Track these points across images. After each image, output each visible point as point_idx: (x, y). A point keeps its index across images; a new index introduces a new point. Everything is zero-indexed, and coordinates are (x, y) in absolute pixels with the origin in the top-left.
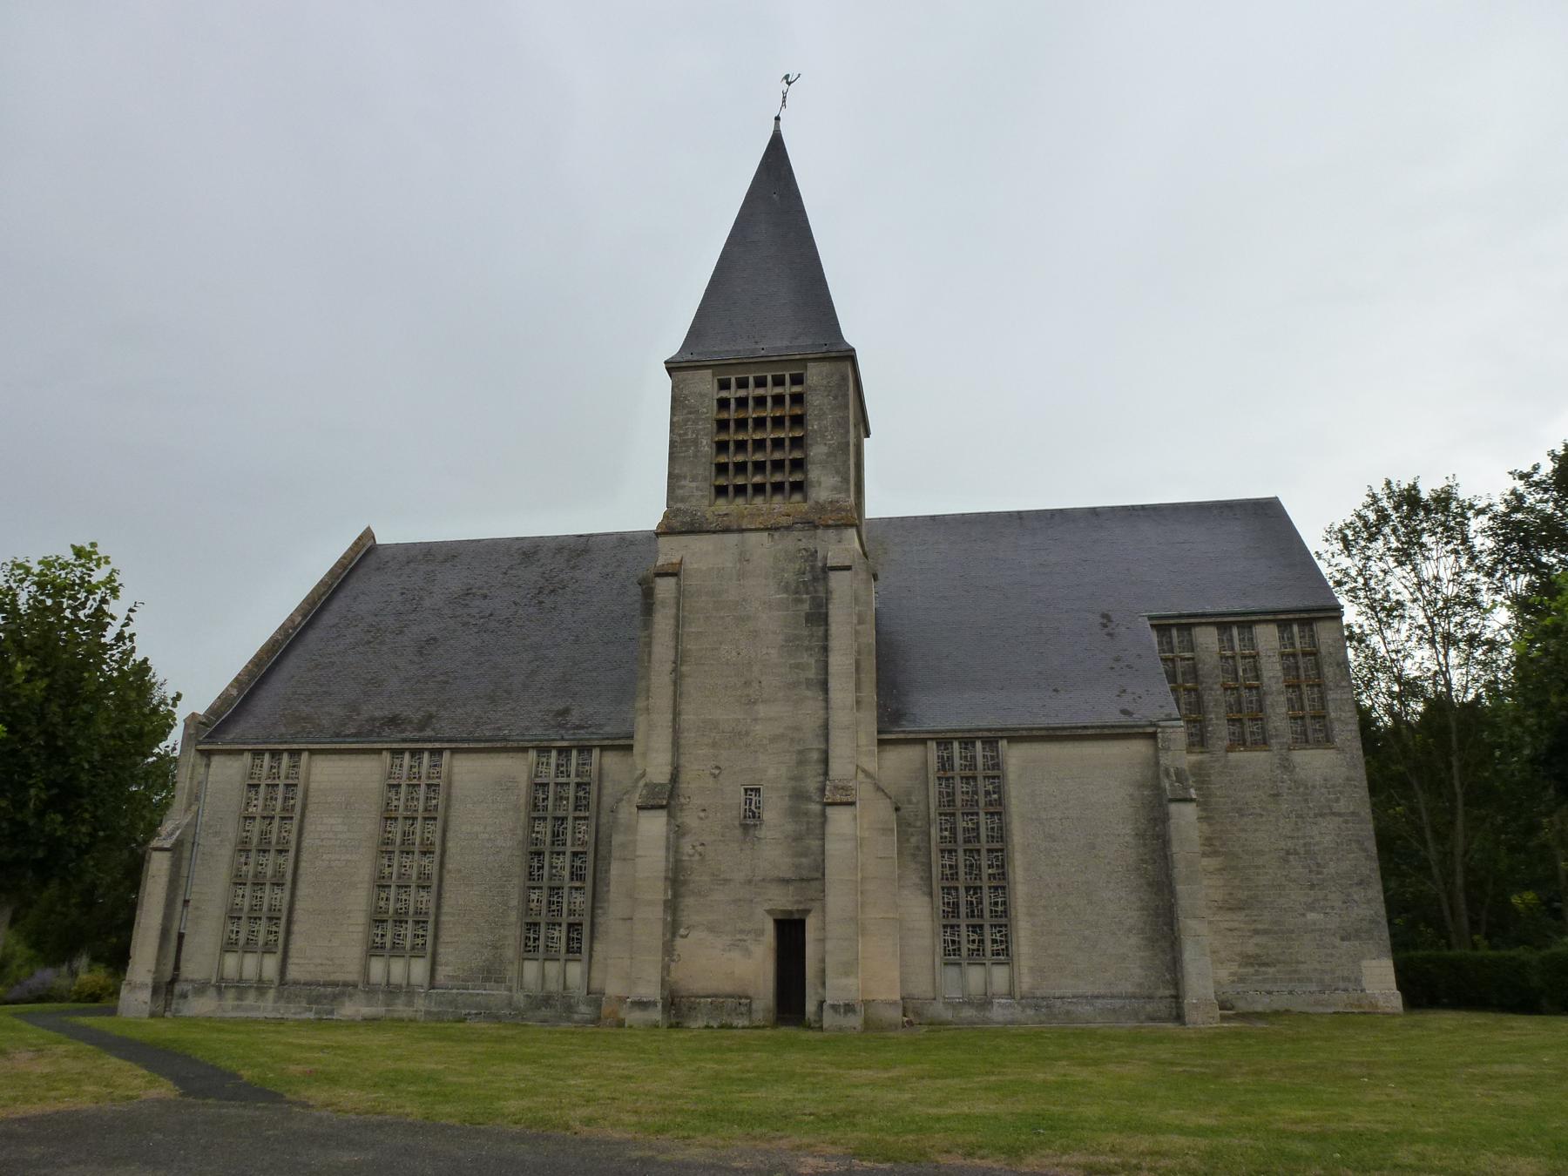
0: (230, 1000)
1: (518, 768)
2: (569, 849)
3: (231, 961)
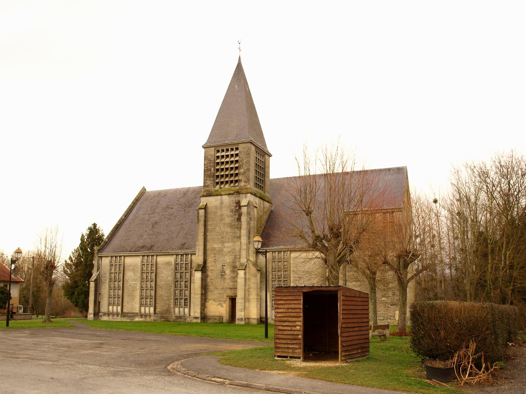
0: (111, 317)
1: (172, 259)
2: (184, 280)
3: (143, 309)
